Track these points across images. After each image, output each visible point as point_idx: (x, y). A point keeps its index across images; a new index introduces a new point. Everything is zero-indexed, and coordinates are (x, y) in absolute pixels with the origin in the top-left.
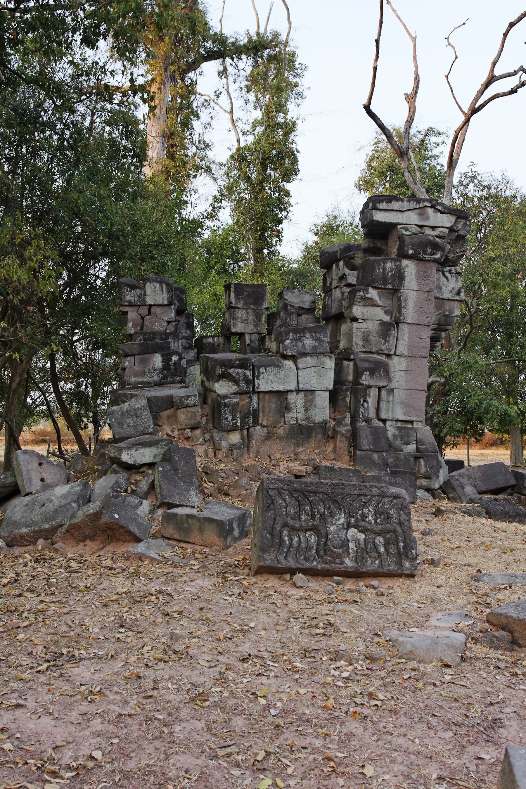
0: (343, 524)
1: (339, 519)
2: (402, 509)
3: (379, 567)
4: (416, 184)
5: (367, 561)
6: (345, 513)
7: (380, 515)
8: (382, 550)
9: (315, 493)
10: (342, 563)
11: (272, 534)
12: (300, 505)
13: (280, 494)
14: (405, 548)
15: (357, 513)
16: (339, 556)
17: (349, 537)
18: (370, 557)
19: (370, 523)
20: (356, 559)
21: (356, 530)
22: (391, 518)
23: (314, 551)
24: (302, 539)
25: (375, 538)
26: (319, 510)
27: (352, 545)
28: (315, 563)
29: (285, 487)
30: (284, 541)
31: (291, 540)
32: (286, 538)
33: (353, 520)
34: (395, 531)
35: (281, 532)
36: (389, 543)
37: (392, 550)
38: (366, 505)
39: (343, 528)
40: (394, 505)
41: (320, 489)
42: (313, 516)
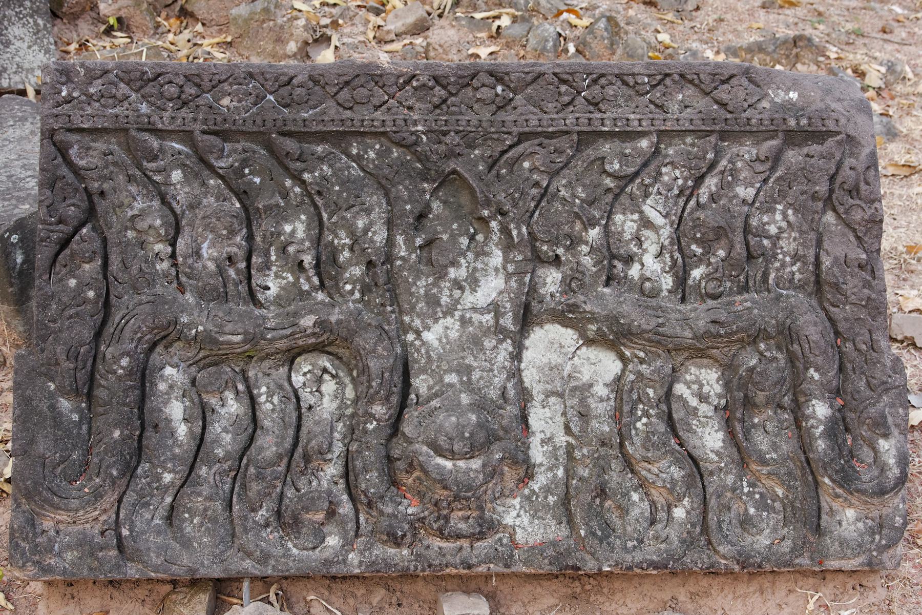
0: (495, 308)
1: (473, 282)
2: (829, 202)
3: (688, 543)
4: (890, 376)
5: (624, 511)
6: (508, 246)
7: (707, 245)
8: (711, 440)
9: (339, 138)
10: (487, 527)
11: (86, 389)
12: (249, 217)
13: (140, 156)
14: (838, 427)
15: (574, 242)
16: (463, 493)
17: (530, 377)
18: (643, 485)
19: (645, 291)
20: (566, 501)
21: (568, 336)
22: (769, 256)
23: (332, 470)
24: (267, 404)
25: (674, 376)
26: (308, 279)
27: (545, 420)
28: (333, 541)
29: (164, 121)
30: (163, 427)
31: (203, 415)
32: (176, 410)
33: (551, 280)
34: (787, 335)
35: (143, 376)
36: (748, 403)
37: (769, 437)
38: (624, 190)
39: (499, 330)
40: (787, 181)
41: (365, 116)
42: (326, 268)
